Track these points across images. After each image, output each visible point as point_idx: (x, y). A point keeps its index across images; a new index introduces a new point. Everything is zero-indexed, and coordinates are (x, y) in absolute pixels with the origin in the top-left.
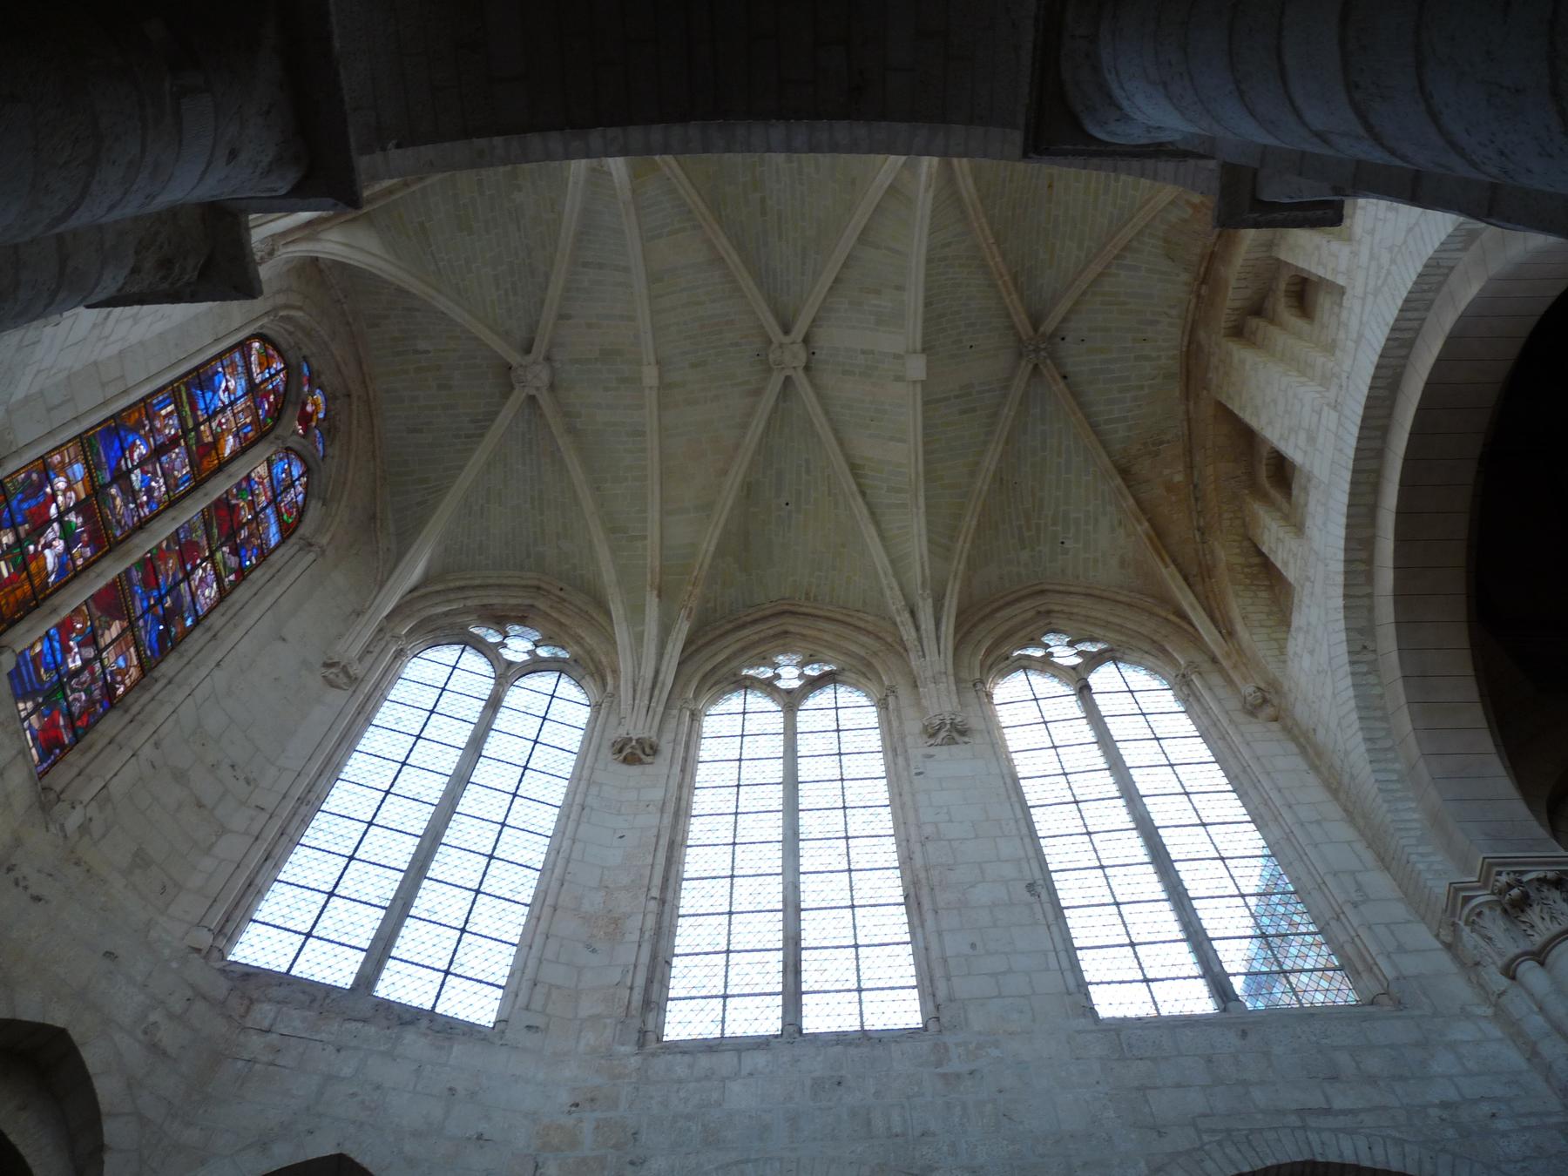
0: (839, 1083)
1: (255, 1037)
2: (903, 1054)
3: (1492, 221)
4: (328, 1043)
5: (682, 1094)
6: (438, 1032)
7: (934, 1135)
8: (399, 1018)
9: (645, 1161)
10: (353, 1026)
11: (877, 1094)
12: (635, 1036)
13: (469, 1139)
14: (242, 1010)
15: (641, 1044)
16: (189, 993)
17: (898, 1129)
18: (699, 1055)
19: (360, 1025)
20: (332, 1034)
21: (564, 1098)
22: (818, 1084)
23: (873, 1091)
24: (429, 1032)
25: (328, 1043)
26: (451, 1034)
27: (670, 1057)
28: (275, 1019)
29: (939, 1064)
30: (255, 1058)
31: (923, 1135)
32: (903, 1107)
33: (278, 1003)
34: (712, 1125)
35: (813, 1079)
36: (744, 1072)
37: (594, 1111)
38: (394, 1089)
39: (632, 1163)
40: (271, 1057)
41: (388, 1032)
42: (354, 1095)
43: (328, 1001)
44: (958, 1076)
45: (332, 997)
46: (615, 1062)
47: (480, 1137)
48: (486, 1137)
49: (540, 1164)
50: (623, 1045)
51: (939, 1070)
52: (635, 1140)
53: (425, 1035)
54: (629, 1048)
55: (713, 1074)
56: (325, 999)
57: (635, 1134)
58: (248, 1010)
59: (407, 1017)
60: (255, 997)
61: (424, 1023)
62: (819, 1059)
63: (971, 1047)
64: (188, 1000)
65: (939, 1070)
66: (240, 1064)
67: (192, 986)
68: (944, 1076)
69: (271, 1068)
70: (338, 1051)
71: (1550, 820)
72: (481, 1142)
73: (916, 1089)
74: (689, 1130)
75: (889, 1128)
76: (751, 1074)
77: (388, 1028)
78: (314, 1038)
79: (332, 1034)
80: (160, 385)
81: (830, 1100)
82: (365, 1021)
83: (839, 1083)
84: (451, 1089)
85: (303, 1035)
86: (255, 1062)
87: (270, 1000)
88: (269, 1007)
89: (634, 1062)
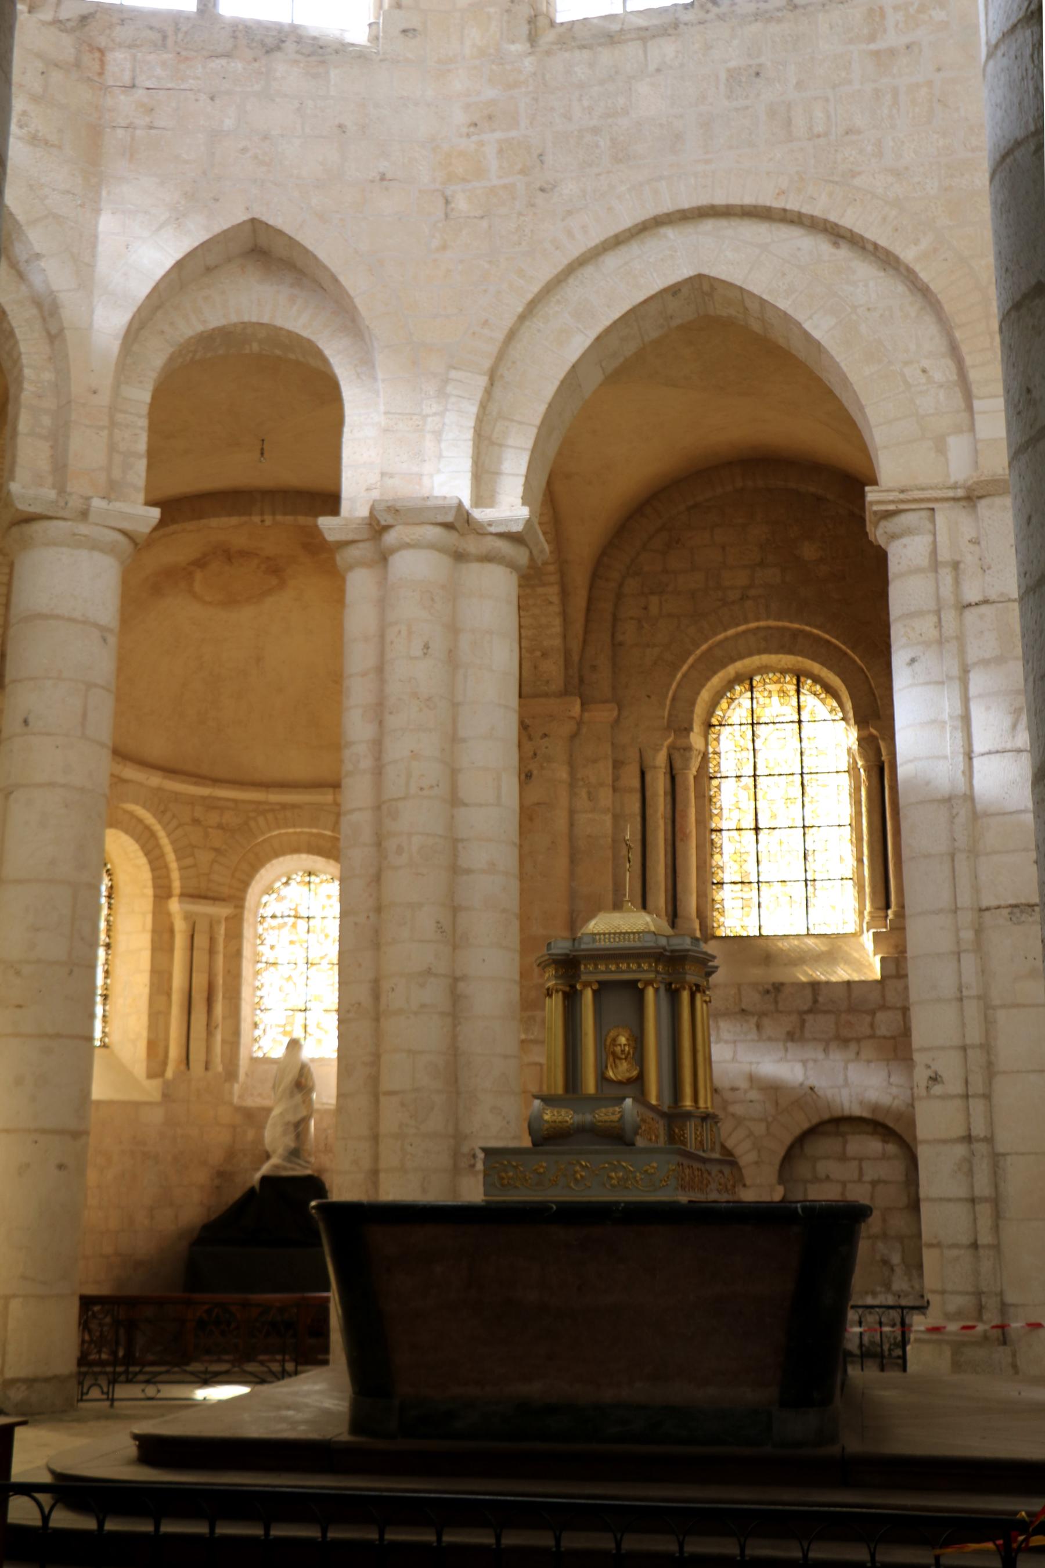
0: (758, 74)
1: (122, 97)
2: (831, 28)
3: (196, 1367)
4: (199, 91)
5: (586, 103)
6: (309, 55)
7: (859, 132)
8: (263, 44)
9: (555, 186)
10: (217, 64)
11: (799, 85)
12: (525, 29)
13: (372, 181)
14: (96, 67)
15: (532, 39)
16: (40, 65)
17: (819, 129)
18: (600, 49)
19: (223, 61)
20: (198, 78)
21: (459, 117)
22: (734, 76)
23: (794, 82)
24: (298, 57)
25: (199, 91)
26: (322, 55)
27: (567, 55)
28: (133, 70)
29: (872, 38)
30: (132, 123)
31: (847, 133)
32: (827, 100)
33: (130, 47)
34: (622, 138)
35: (728, 70)
36: (652, 68)
37: (493, 131)
38: (282, 136)
39: (542, 190)
40: (148, 119)
41: (256, 65)
42: (244, 150)
43: (180, 36)
44: (892, 52)
45: (184, 29)
46: (508, 67)
47: (383, 178)
48: (388, 176)
49: (450, 199)
50: (513, 42)
51: (872, 47)
52: (542, 162)
53: (296, 62)
54: (520, 47)
55: (617, 72)
56: (176, 34)
57: (541, 155)
58: (102, 63)
59: (269, 41)
60: (103, 45)
61: (290, 46)
62: (736, 42)
63: (912, 10)
64: (43, 73)
65: (872, 47)
66: (120, 132)
67: (39, 56)
68: (877, 54)
69: (153, 132)
70: (212, 99)
71: (1026, 297)
72: (385, 183)
73: (843, 74)
74: (597, 146)
75: (810, 128)
76: (658, 70)
77: (255, 60)
78: (182, 87)
79: (198, 78)
80: (699, 924)
81: (747, 97)
82: (228, 55)
83: (758, 74)
84: (340, 126)
85: (170, 86)
86: (135, 128)
87: (120, 45)
88: (122, 56)
89: (528, 64)
